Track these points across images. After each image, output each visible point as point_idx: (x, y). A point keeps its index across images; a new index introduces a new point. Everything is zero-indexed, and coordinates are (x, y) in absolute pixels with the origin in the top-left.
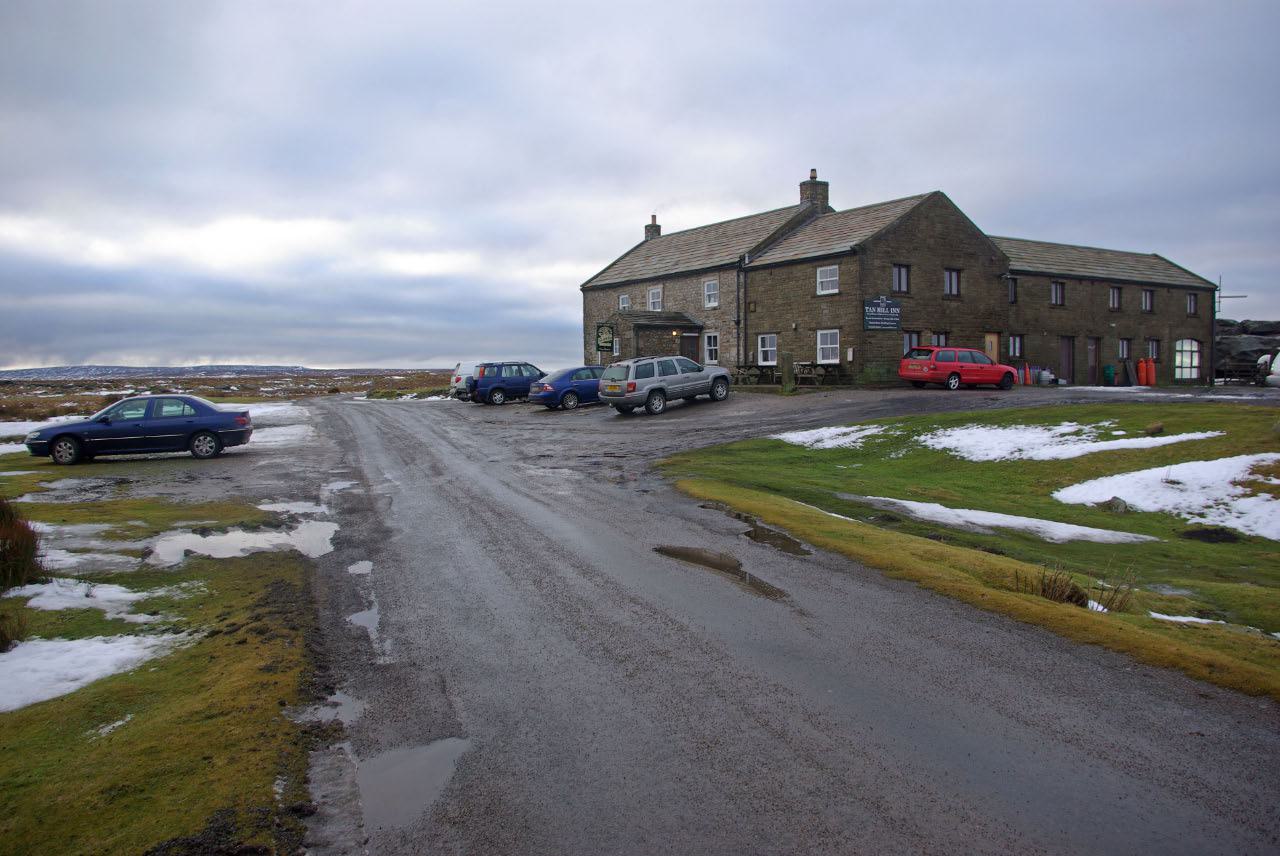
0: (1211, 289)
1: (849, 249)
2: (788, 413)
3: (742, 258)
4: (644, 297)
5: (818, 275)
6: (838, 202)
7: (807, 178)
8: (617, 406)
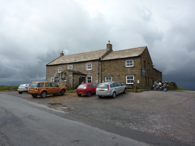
2: (58, 93)
3: (100, 58)
4: (67, 67)
5: (126, 62)
6: (114, 49)
8: (32, 94)
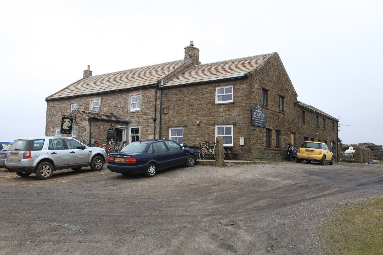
0: (335, 122)
1: (243, 75)
3: (159, 82)
4: (88, 104)
6: (204, 59)
7: (188, 45)
